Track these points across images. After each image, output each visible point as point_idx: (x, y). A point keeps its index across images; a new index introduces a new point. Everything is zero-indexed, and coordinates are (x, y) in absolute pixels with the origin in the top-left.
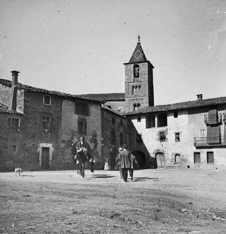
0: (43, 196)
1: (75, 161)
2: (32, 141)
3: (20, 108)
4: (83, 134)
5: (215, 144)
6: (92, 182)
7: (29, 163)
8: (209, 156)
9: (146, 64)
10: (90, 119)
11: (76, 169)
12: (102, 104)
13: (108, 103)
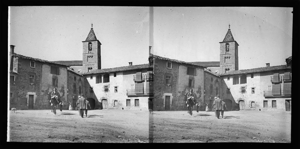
0: (29, 126)
1: (50, 103)
2: (23, 91)
3: (15, 69)
4: (56, 86)
5: (140, 94)
6: (61, 117)
7: (20, 105)
8: (273, 103)
9: (97, 42)
10: (60, 77)
11: (50, 109)
12: (68, 68)
13: (208, 68)
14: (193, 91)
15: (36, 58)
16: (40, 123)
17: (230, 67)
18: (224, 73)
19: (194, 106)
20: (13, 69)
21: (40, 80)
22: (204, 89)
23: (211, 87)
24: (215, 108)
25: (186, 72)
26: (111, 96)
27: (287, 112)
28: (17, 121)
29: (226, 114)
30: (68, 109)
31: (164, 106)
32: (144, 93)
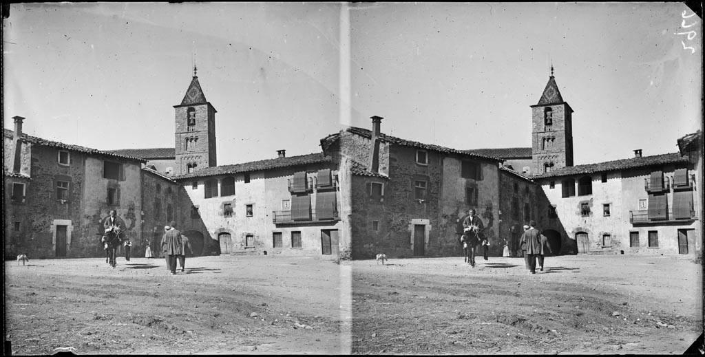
1: (462, 244)
2: (401, 216)
8: (295, 238)
10: (482, 184)
12: (500, 164)
13: (151, 163)
14: (118, 215)
15: (430, 144)
16: (440, 286)
17: (197, 160)
18: (184, 173)
19: (120, 247)
20: (378, 167)
21: (439, 190)
22: (141, 208)
23: (157, 205)
24: (165, 251)
25: (101, 172)
26: (597, 224)
27: (324, 255)
28: (389, 284)
29: (190, 262)
30: (501, 255)
31: (54, 248)
32: (667, 218)
